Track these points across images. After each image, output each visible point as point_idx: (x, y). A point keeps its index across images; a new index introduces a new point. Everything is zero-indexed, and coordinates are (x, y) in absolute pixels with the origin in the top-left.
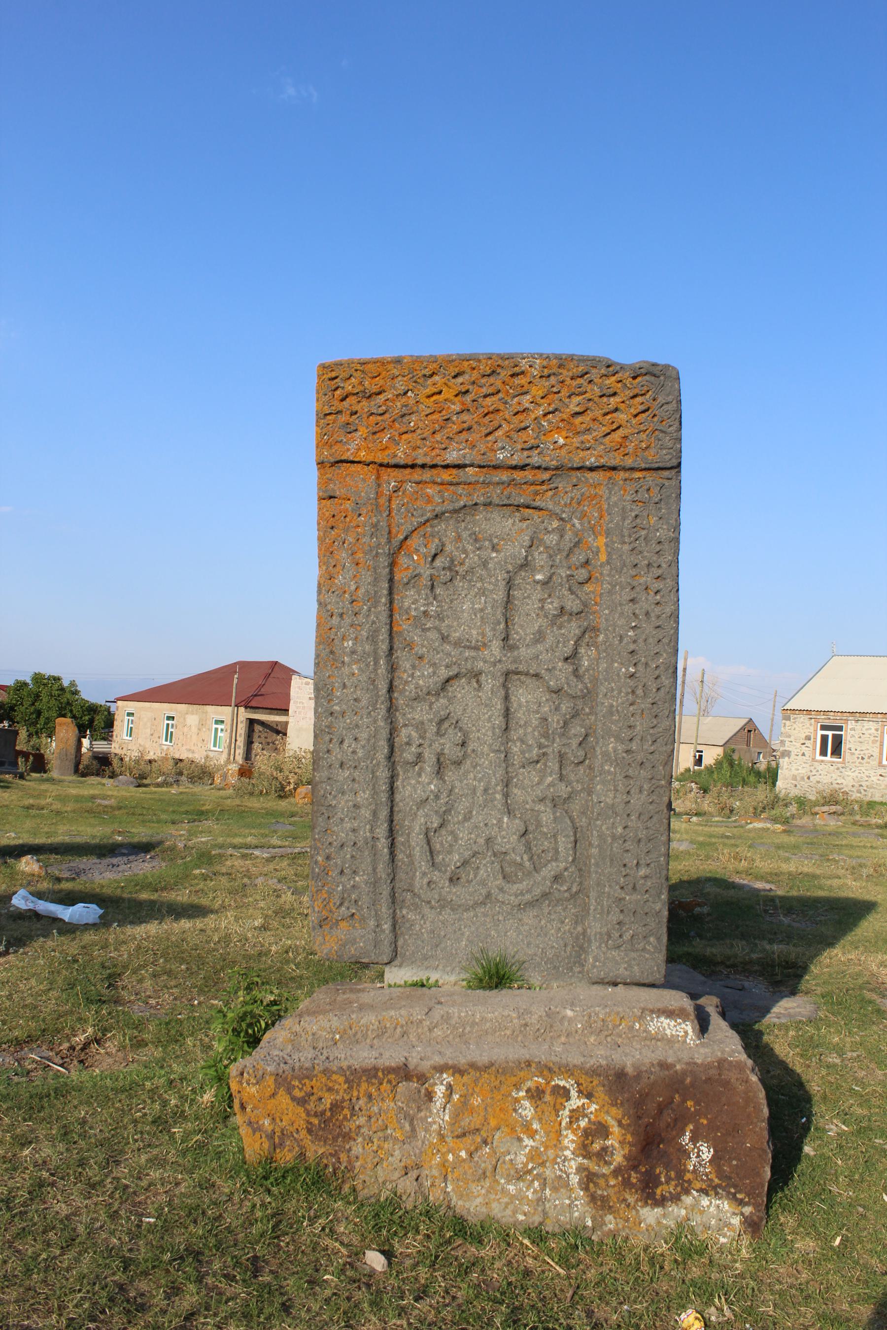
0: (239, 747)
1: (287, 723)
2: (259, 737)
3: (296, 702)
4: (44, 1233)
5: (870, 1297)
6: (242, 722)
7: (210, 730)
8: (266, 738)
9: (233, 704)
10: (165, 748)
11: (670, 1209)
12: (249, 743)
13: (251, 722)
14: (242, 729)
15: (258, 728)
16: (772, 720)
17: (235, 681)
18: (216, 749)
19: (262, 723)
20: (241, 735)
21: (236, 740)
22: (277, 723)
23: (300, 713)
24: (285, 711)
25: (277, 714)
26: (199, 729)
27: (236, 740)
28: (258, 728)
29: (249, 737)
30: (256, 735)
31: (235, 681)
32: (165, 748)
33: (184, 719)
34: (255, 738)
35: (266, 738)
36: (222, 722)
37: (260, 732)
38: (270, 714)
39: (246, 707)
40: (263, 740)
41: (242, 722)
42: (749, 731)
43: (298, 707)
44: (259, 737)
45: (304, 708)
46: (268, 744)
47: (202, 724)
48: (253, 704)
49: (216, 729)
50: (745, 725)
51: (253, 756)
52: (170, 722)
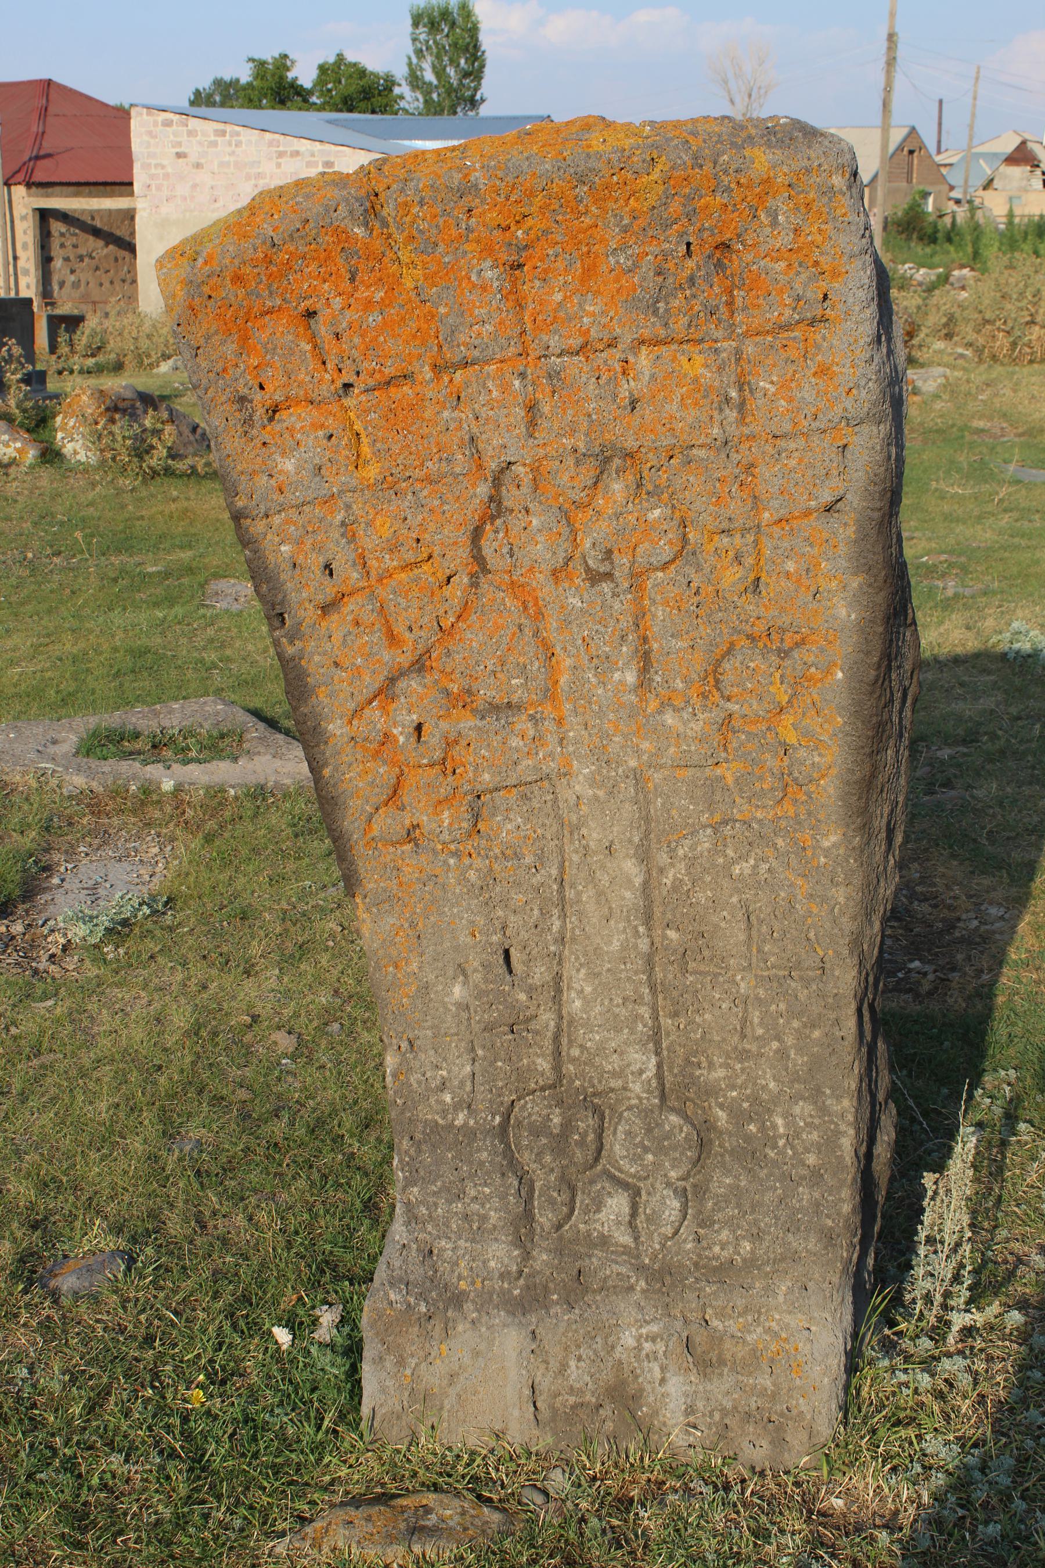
0: (26, 273)
1: (130, 215)
2: (62, 246)
3: (146, 166)
6: (24, 218)
8: (75, 246)
11: (395, 563)
12: (45, 260)
13: (44, 216)
14: (26, 232)
15: (57, 227)
16: (971, 127)
19: (64, 217)
20: (25, 246)
21: (15, 258)
22: (93, 214)
23: (159, 188)
24: (125, 186)
25: (90, 195)
27: (15, 258)
28: (57, 227)
29: (43, 247)
30: (55, 243)
35: (75, 246)
37: (62, 235)
38: (76, 195)
39: (29, 185)
41: (24, 218)
42: (911, 152)
43: (152, 177)
44: (62, 246)
45: (167, 176)
46: (81, 258)
48: (39, 176)
50: (905, 140)
51: (56, 287)
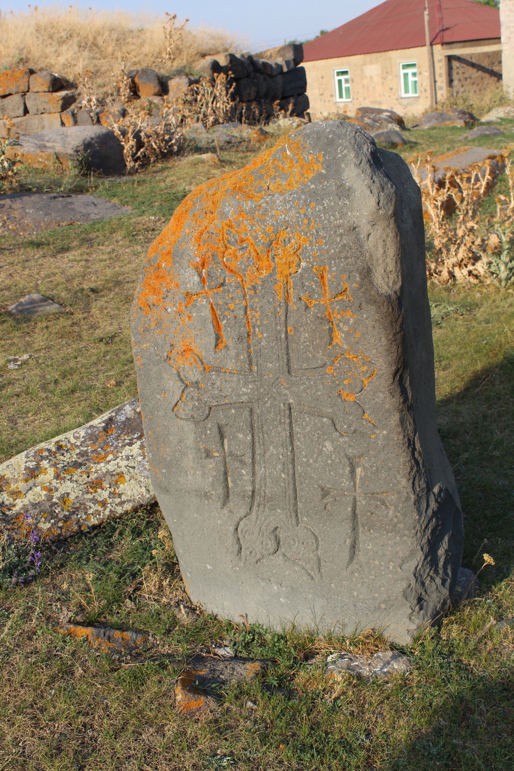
0: (441, 88)
1: (498, 54)
2: (458, 73)
4: (104, 357)
5: (130, 174)
6: (440, 61)
7: (398, 76)
8: (463, 73)
9: (428, 42)
10: (342, 105)
13: (450, 59)
14: (441, 68)
17: (426, 18)
18: (411, 94)
19: (458, 59)
20: (440, 75)
24: (498, 39)
26: (384, 78)
28: (455, 64)
31: (426, 18)
32: (342, 105)
33: (362, 71)
34: (455, 77)
35: (463, 73)
36: (414, 65)
37: (458, 68)
38: (464, 47)
39: (443, 44)
40: (461, 76)
41: (440, 61)
46: (466, 79)
47: (386, 72)
48: (447, 40)
49: (406, 75)
52: (343, 78)
